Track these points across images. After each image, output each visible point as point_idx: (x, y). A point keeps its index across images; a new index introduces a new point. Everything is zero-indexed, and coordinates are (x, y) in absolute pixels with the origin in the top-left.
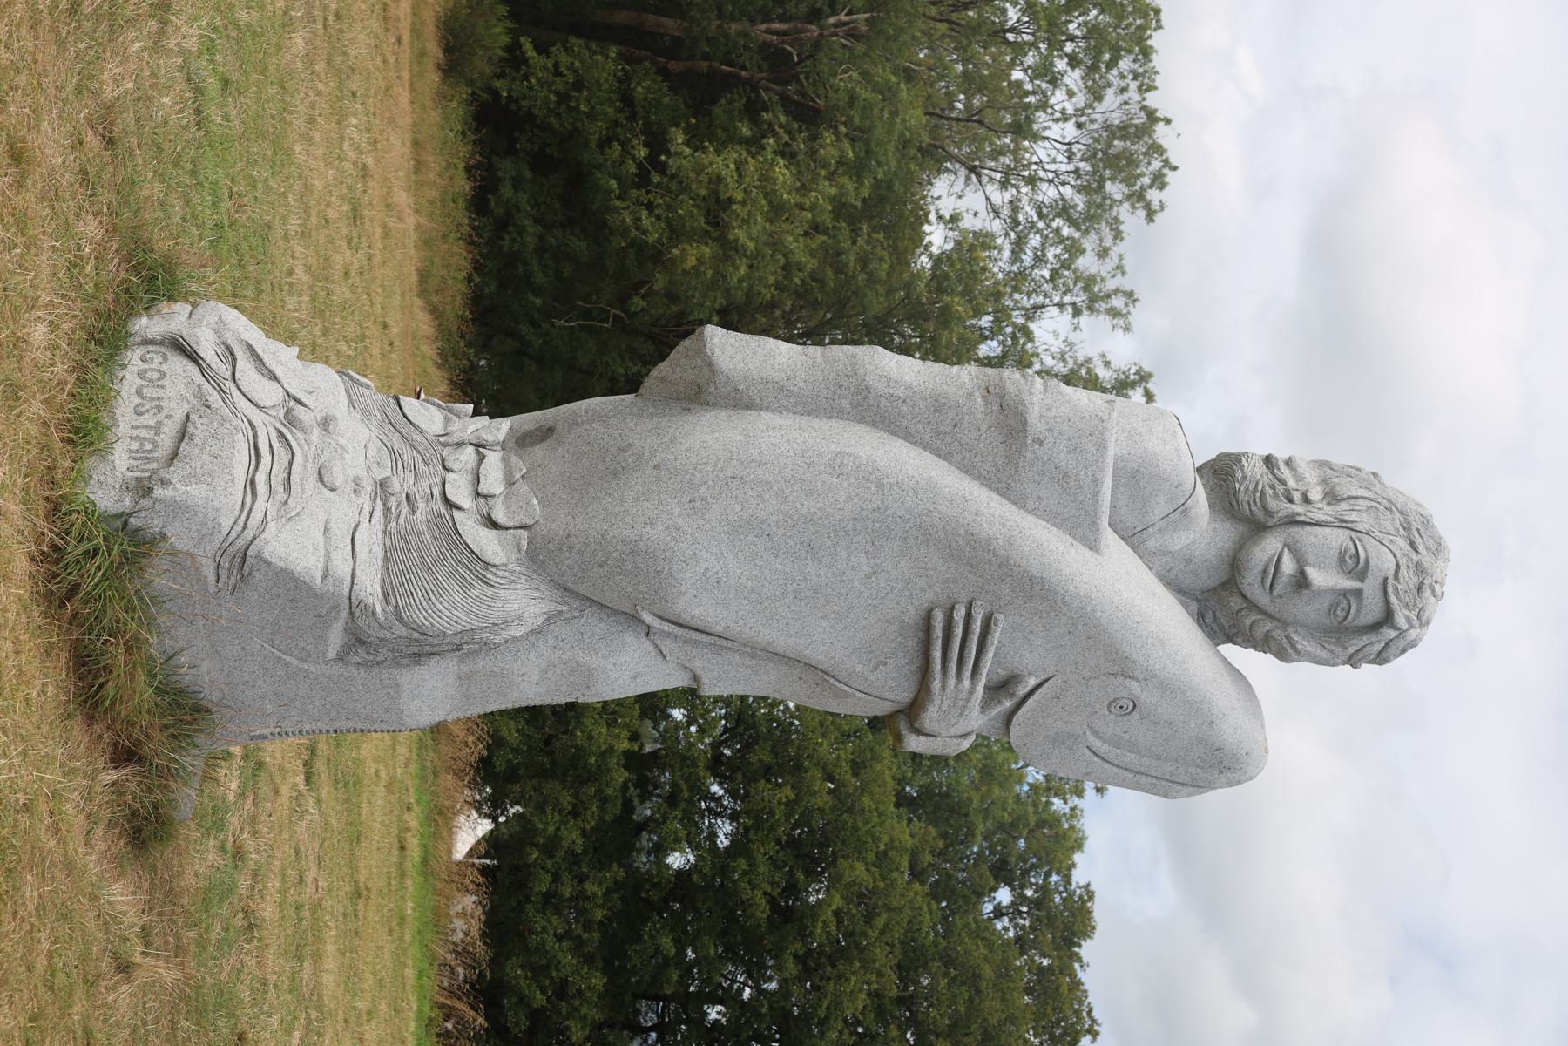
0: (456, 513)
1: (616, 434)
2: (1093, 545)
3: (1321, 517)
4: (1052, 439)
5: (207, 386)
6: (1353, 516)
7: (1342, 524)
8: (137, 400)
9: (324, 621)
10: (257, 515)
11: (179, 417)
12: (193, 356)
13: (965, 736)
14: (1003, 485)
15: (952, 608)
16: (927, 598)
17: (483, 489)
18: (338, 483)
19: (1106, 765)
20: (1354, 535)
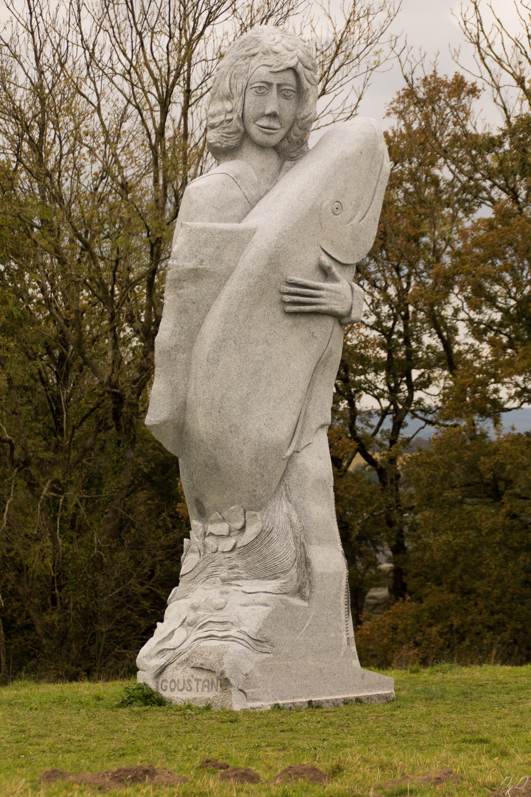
0: (239, 545)
1: (199, 468)
2: (253, 232)
3: (240, 104)
4: (200, 256)
5: (178, 661)
6: (240, 87)
7: (244, 93)
8: (185, 691)
9: (288, 606)
10: (238, 635)
11: (192, 672)
12: (163, 669)
13: (352, 289)
14: (223, 279)
15: (285, 302)
16: (279, 314)
17: (225, 533)
18: (223, 601)
19: (370, 210)
20: (249, 87)
